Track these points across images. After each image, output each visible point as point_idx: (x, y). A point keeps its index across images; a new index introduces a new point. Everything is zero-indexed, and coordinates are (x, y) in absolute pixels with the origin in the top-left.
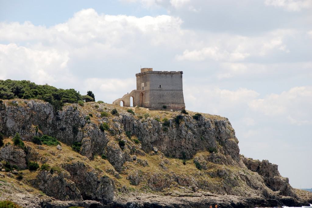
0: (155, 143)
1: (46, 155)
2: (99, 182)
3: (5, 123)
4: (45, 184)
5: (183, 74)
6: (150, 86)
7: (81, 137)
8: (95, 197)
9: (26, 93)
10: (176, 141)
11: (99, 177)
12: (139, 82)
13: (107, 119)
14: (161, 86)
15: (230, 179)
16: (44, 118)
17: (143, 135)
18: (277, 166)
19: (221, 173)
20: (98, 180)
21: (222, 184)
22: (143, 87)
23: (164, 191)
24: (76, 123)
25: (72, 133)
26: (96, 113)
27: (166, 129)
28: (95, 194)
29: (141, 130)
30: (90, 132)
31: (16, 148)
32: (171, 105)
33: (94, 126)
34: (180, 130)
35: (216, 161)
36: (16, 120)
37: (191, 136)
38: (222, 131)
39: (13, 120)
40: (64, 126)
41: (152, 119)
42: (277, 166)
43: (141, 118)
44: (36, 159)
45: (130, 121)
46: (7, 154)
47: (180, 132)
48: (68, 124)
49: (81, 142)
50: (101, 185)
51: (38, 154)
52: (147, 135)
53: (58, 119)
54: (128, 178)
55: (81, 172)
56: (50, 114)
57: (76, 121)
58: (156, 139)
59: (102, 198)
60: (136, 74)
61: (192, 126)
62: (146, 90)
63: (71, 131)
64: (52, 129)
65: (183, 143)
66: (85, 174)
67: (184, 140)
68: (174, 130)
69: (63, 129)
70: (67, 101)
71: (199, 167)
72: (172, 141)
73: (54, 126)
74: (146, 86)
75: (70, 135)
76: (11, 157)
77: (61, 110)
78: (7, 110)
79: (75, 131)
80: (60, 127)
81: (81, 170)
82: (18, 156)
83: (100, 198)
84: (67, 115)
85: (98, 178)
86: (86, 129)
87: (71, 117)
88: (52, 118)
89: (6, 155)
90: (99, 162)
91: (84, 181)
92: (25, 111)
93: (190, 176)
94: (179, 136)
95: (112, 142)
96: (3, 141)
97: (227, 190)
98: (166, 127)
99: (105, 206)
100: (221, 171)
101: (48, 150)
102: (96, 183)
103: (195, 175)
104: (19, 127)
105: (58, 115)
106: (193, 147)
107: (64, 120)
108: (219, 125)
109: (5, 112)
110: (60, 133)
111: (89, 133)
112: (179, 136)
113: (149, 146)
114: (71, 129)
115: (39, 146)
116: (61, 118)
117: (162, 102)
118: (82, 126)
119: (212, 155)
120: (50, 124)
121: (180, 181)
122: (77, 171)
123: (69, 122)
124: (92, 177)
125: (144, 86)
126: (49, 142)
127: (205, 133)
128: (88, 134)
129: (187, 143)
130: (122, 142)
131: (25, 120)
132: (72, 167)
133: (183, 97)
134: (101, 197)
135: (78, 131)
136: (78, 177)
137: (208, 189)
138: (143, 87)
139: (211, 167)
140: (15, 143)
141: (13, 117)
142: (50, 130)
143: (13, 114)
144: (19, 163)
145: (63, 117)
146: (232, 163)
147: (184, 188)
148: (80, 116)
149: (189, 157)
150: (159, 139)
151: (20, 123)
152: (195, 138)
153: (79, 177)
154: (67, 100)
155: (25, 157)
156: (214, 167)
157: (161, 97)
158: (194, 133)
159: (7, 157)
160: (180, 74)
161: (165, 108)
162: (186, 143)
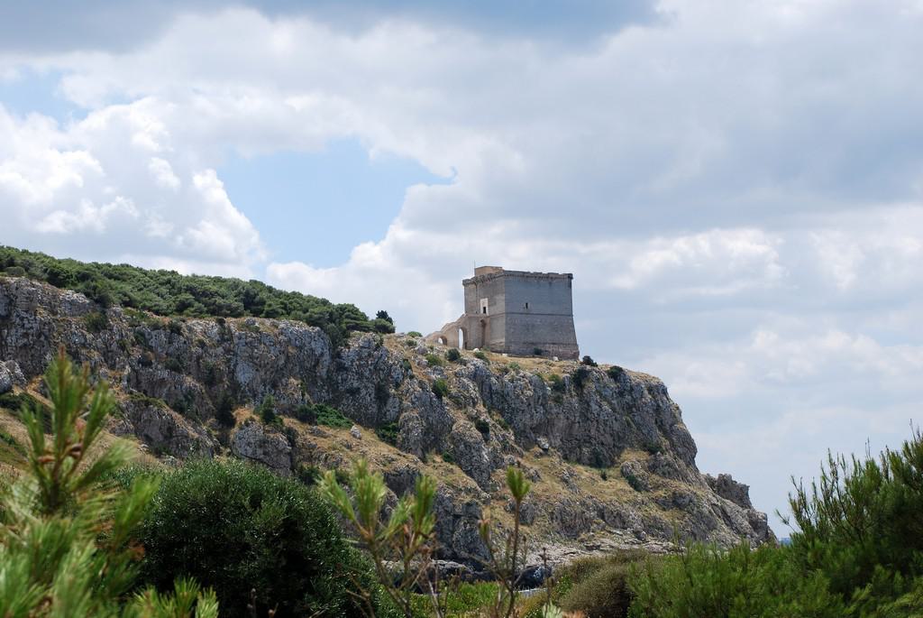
0: (537, 429)
1: (334, 449)
2: (457, 517)
6: (507, 304)
7: (397, 410)
8: (450, 552)
9: (270, 305)
11: (456, 503)
12: (473, 297)
13: (441, 370)
15: (701, 513)
17: (514, 411)
18: (747, 488)
19: (681, 500)
20: (456, 510)
21: (687, 525)
22: (485, 308)
23: (582, 541)
24: (382, 377)
25: (374, 400)
26: (416, 357)
27: (559, 397)
28: (451, 546)
29: (508, 398)
30: (415, 397)
31: (268, 432)
32: (550, 348)
33: (421, 384)
34: (586, 401)
35: (664, 473)
36: (256, 364)
39: (251, 364)
40: (356, 384)
41: (529, 374)
42: (747, 488)
43: (506, 371)
44: (310, 459)
46: (249, 444)
47: (586, 405)
48: (365, 380)
49: (396, 421)
50: (465, 523)
51: (315, 446)
52: (523, 411)
53: (341, 368)
54: (509, 508)
56: (322, 354)
58: (541, 420)
60: (464, 281)
61: (609, 393)
62: (492, 313)
63: (373, 395)
64: (327, 391)
65: (593, 432)
67: (595, 423)
68: (575, 400)
69: (354, 392)
70: (356, 327)
71: (635, 484)
72: (571, 426)
73: (330, 383)
74: (495, 304)
76: (260, 451)
77: (347, 346)
78: (236, 341)
79: (382, 397)
80: (347, 386)
83: (464, 554)
84: (360, 359)
85: (454, 506)
86: (407, 392)
90: (441, 471)
92: (275, 344)
93: (626, 506)
94: (585, 415)
95: (461, 423)
96: (234, 414)
98: (559, 393)
100: (681, 496)
101: (335, 437)
102: (451, 518)
103: (635, 503)
104: (264, 382)
105: (340, 357)
106: (614, 440)
108: (656, 393)
109: (232, 346)
110: (347, 399)
111: (414, 400)
112: (585, 415)
113: (527, 437)
114: (372, 390)
115: (315, 427)
116: (348, 364)
117: (531, 340)
118: (397, 386)
119: (656, 460)
120: (322, 380)
121: (609, 517)
123: (367, 374)
124: (440, 503)
125: (489, 306)
126: (331, 419)
127: (634, 409)
128: (413, 403)
129: (602, 432)
130: (483, 424)
131: (275, 366)
132: (394, 480)
135: (389, 397)
137: (663, 536)
138: (485, 308)
139: (657, 487)
140: (264, 418)
141: (251, 357)
142: (324, 394)
143: (249, 350)
145: (352, 362)
146: (689, 478)
147: (621, 533)
149: (609, 464)
151: (266, 373)
152: (616, 419)
154: (357, 324)
155: (290, 454)
156: (664, 485)
157: (528, 329)
158: (614, 410)
161: (538, 353)
162: (599, 431)
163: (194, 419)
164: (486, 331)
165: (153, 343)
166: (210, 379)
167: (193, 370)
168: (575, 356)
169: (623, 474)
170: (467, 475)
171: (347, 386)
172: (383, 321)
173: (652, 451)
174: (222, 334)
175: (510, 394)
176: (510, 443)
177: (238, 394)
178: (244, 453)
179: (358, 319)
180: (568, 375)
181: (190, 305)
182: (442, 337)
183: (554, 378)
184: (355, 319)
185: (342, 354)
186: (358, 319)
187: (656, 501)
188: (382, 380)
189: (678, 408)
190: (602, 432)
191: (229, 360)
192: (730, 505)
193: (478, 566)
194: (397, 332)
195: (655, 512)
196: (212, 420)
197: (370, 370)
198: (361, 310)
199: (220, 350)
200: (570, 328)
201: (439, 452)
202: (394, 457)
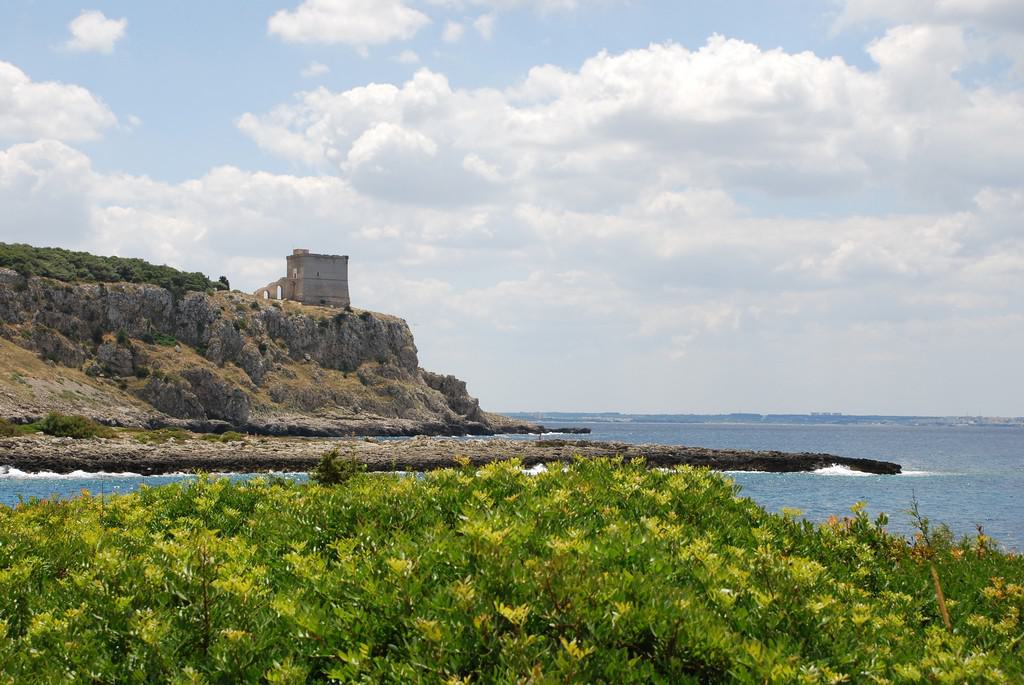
0: (307, 348)
2: (229, 397)
15: (404, 399)
17: (292, 338)
18: (464, 383)
32: (331, 299)
33: (226, 322)
40: (186, 321)
42: (464, 383)
43: (291, 314)
44: (146, 363)
46: (107, 354)
53: (178, 312)
61: (357, 328)
65: (345, 350)
69: (184, 325)
70: (192, 288)
73: (171, 320)
76: (113, 358)
77: (183, 299)
79: (200, 328)
95: (250, 346)
104: (125, 320)
117: (320, 294)
118: (210, 322)
139: (379, 383)
158: (360, 338)
161: (323, 303)
163: (75, 339)
165: (55, 297)
166: (91, 317)
167: (80, 312)
169: (359, 375)
173: (381, 362)
174: (101, 292)
177: (108, 326)
181: (86, 275)
183: (323, 319)
187: (376, 391)
191: (104, 307)
193: (237, 423)
195: (374, 397)
196: (90, 340)
199: (99, 301)
200: (346, 288)
201: (233, 361)
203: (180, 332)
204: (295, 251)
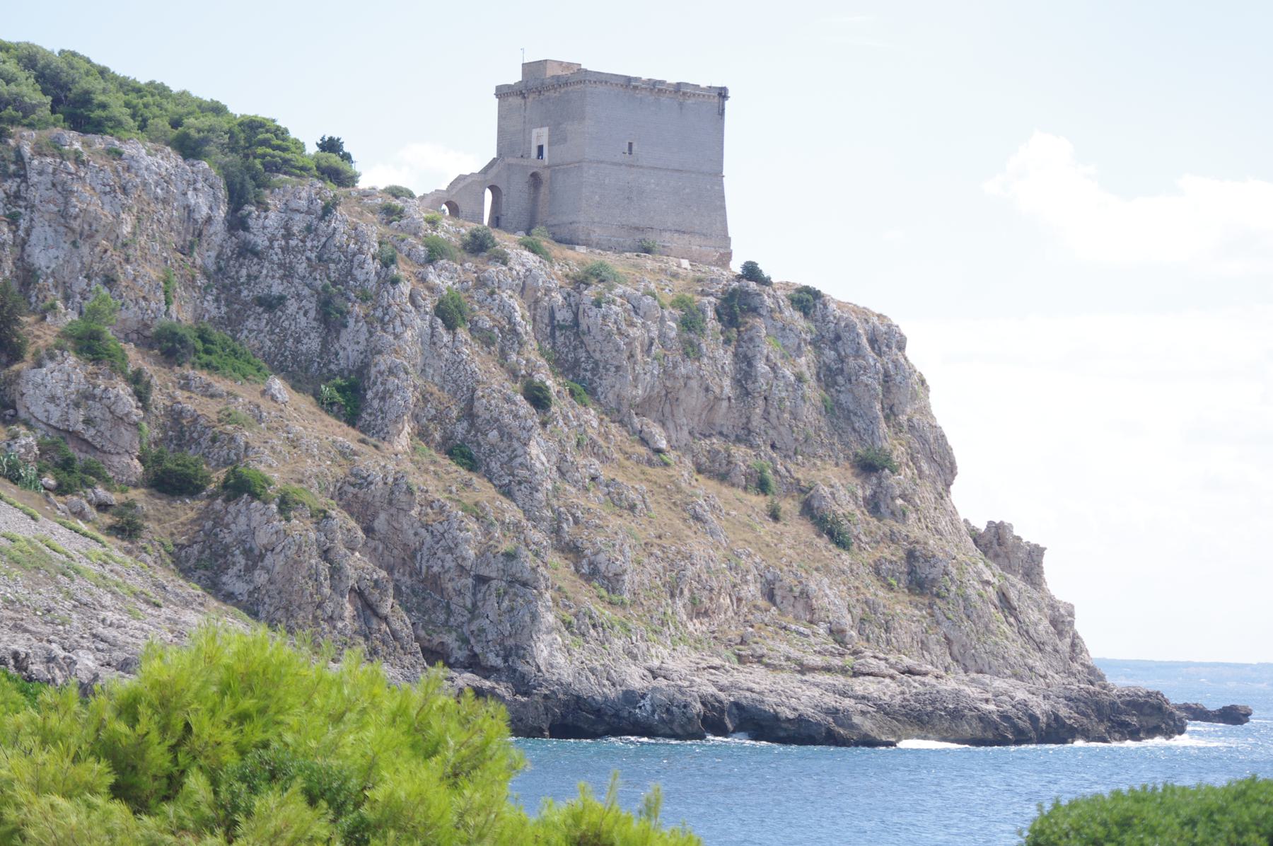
3: (24, 242)
4: (257, 572)
5: (726, 102)
10: (730, 407)
14: (635, 148)
16: (185, 241)
22: (540, 148)
29: (586, 339)
36: (73, 231)
37: (790, 389)
38: (899, 378)
39: (62, 229)
40: (277, 288)
45: (539, 294)
48: (296, 281)
53: (247, 251)
55: (396, 525)
57: (332, 266)
58: (652, 388)
59: (506, 660)
63: (312, 314)
66: (411, 532)
67: (761, 402)
69: (271, 304)
74: (565, 140)
75: (307, 334)
81: (393, 511)
82: (108, 416)
83: (494, 660)
84: (288, 235)
87: (309, 244)
88: (219, 242)
89: (51, 407)
91: (408, 569)
97: (955, 648)
99: (524, 705)
102: (470, 581)
105: (246, 228)
107: (275, 258)
114: (311, 305)
116: (261, 242)
117: (635, 221)
121: (784, 598)
122: (375, 516)
123: (302, 268)
125: (550, 144)
127: (840, 379)
132: (355, 496)
133: (724, 208)
134: (497, 655)
136: (375, 549)
138: (540, 148)
144: (110, 452)
148: (352, 246)
150: (664, 392)
153: (381, 547)
154: (286, 161)
159: (56, 414)
160: (716, 100)
162: (768, 420)
164: (541, 197)
168: (725, 259)
170: (504, 494)
171: (261, 290)
172: (334, 159)
175: (593, 332)
176: (590, 431)
178: (43, 418)
179: (285, 150)
180: (712, 299)
182: (448, 204)
184: (278, 148)
185: (251, 222)
186: (285, 150)
188: (334, 284)
189: (923, 382)
190: (775, 421)
192: (1017, 587)
194: (363, 184)
197: (308, 259)
198: (175, 88)
202: (355, 446)
203: (256, 326)
204: (527, 67)
